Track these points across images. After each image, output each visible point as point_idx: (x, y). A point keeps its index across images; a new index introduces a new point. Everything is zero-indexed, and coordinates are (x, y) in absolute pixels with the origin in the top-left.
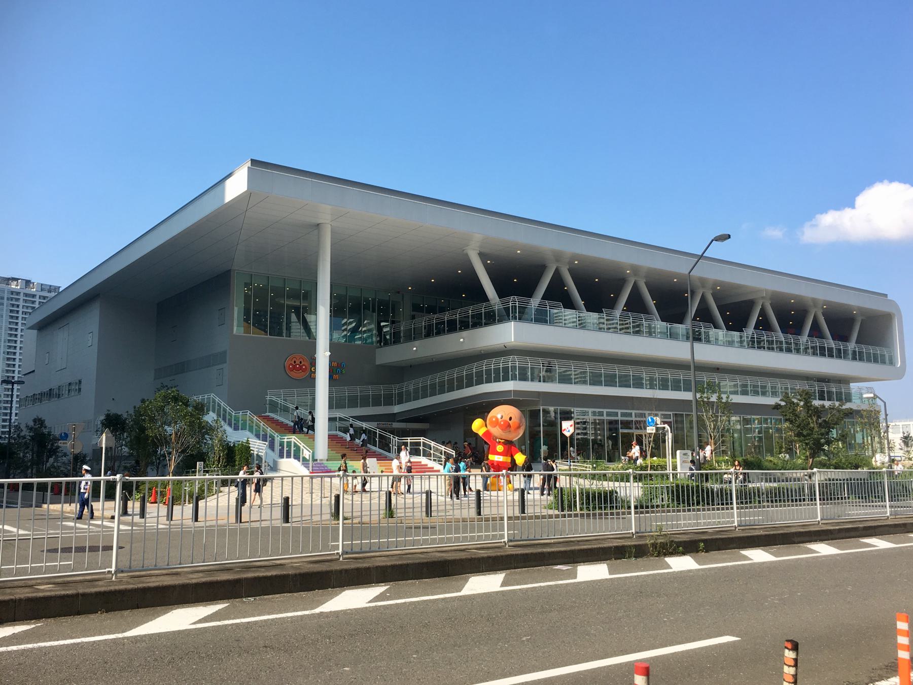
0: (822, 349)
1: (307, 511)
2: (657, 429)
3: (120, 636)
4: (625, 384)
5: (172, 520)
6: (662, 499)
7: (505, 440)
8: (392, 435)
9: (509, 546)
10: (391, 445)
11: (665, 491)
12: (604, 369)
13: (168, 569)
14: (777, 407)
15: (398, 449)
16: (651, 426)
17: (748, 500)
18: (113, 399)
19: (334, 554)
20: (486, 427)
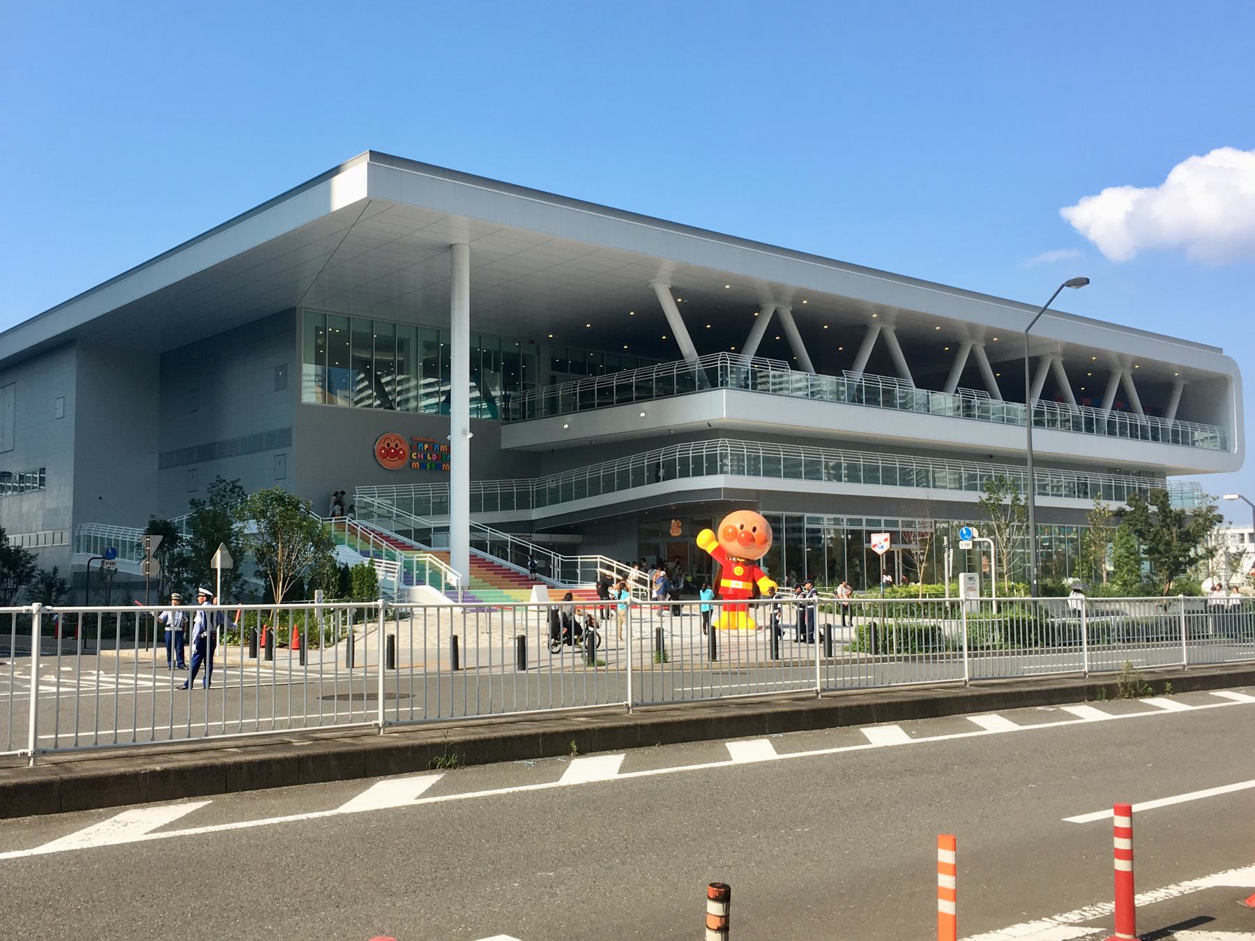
0: (1134, 427)
1: (418, 661)
2: (974, 543)
3: (327, 813)
4: (889, 480)
5: (353, 667)
6: (993, 637)
7: (746, 559)
8: (552, 552)
9: (822, 697)
10: (552, 567)
11: (996, 626)
12: (804, 453)
13: (703, 701)
14: (1120, 513)
15: (561, 571)
16: (967, 539)
17: (1096, 640)
18: (100, 498)
19: (371, 725)
20: (717, 540)
